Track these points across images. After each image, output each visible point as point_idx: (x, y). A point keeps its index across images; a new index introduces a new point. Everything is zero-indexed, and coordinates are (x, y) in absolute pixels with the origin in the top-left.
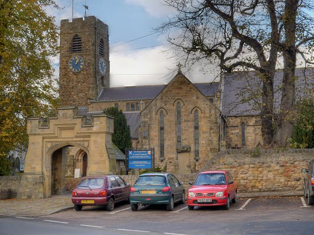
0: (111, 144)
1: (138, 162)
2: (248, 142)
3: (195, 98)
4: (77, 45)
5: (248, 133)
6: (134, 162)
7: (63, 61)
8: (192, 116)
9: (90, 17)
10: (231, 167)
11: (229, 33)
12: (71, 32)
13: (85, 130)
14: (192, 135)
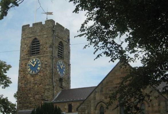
7: (22, 64)
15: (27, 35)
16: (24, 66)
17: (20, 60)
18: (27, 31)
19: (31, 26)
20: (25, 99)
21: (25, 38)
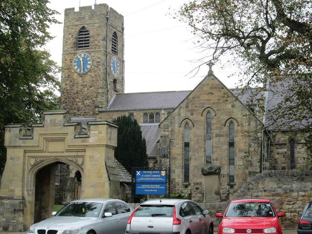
0: (113, 162)
1: (148, 186)
2: (298, 165)
3: (230, 106)
4: (84, 39)
5: (299, 152)
6: (143, 186)
7: (66, 60)
8: (226, 129)
9: (100, 5)
10: (273, 195)
11: (273, 16)
12: (77, 23)
13: (78, 142)
14: (226, 154)
15: (72, 22)
16: (68, 62)
17: (63, 55)
18: (71, 16)
19: (77, 10)
20: (71, 104)
21: (69, 26)
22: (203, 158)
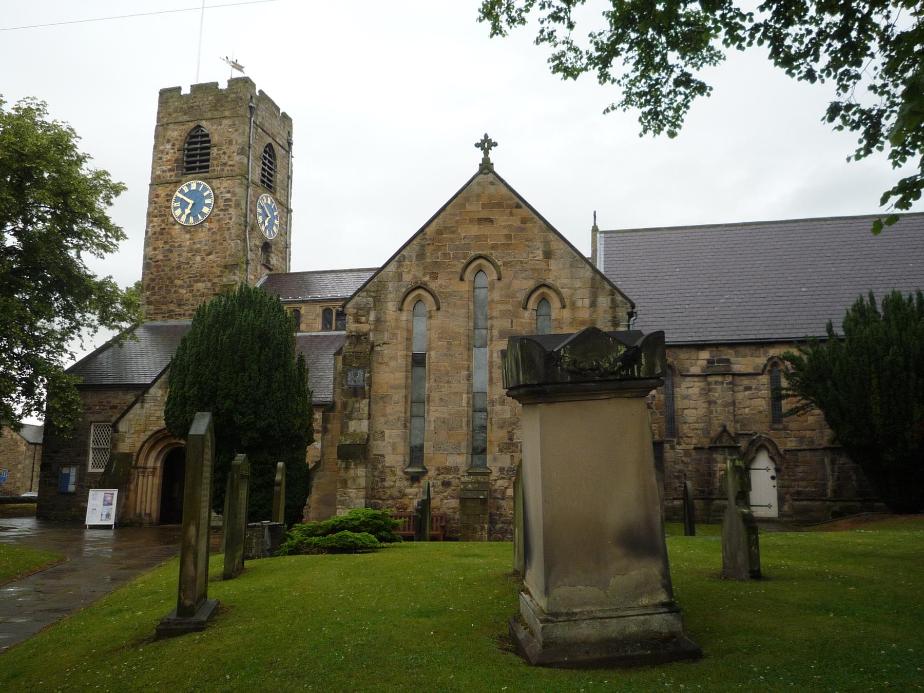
2: (685, 427)
12: (186, 118)
18: (174, 104)
22: (465, 396)
